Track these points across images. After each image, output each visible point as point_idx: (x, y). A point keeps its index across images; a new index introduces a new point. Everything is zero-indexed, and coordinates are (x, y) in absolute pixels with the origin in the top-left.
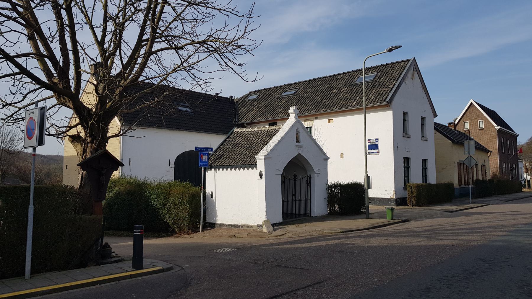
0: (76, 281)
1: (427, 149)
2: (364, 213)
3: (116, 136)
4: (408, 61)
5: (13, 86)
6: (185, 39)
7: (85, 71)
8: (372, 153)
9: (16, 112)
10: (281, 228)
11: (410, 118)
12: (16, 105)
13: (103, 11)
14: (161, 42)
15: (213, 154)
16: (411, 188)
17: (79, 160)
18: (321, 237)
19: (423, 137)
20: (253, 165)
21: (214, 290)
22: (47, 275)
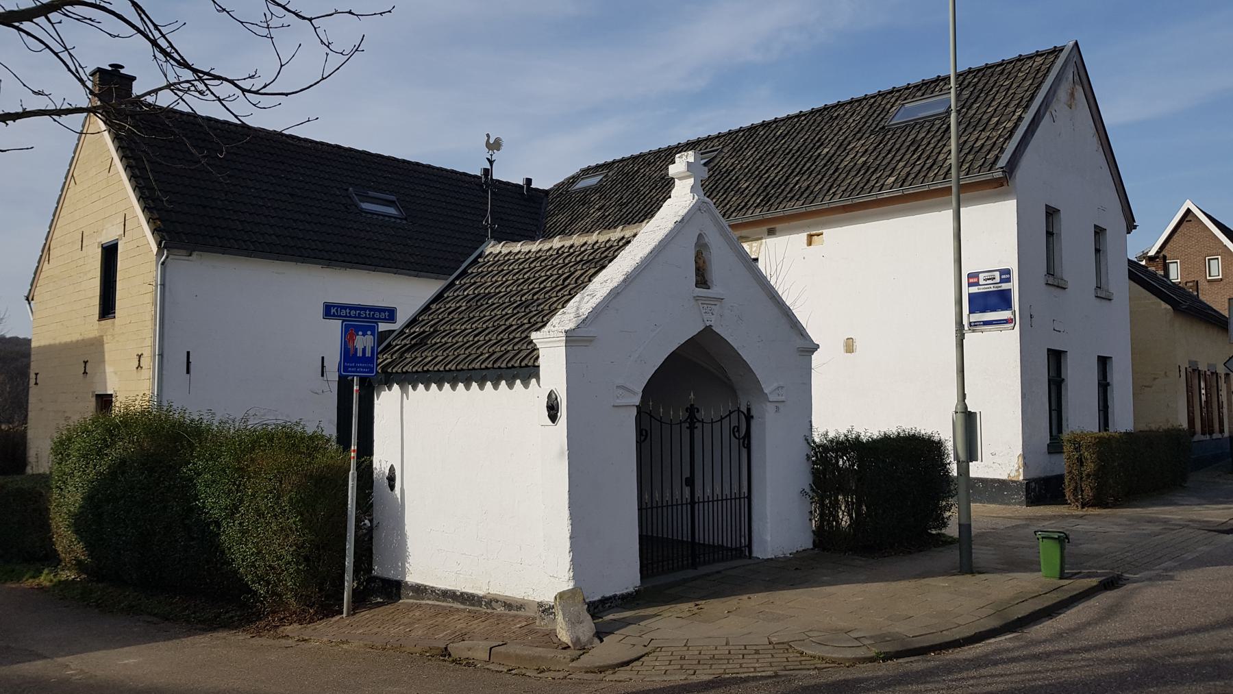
1: (1108, 327)
4: (1056, 51)
8: (986, 323)
10: (625, 623)
11: (1066, 224)
16: (1077, 449)
19: (1102, 294)
20: (524, 368)
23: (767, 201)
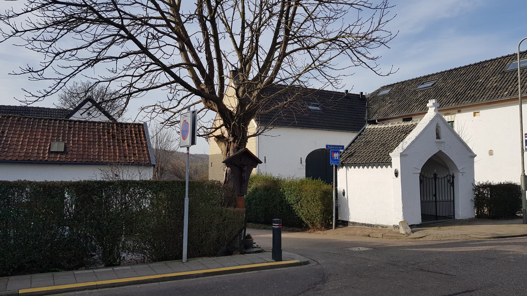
0: (225, 267)
2: (521, 217)
3: (254, 135)
5: (171, 93)
6: (316, 38)
7: (227, 77)
9: (172, 117)
12: (172, 110)
13: (241, 20)
14: (293, 43)
15: (344, 152)
17: (223, 158)
18: (467, 242)
20: (387, 163)
21: (353, 287)
22: (200, 260)
23: (457, 100)
